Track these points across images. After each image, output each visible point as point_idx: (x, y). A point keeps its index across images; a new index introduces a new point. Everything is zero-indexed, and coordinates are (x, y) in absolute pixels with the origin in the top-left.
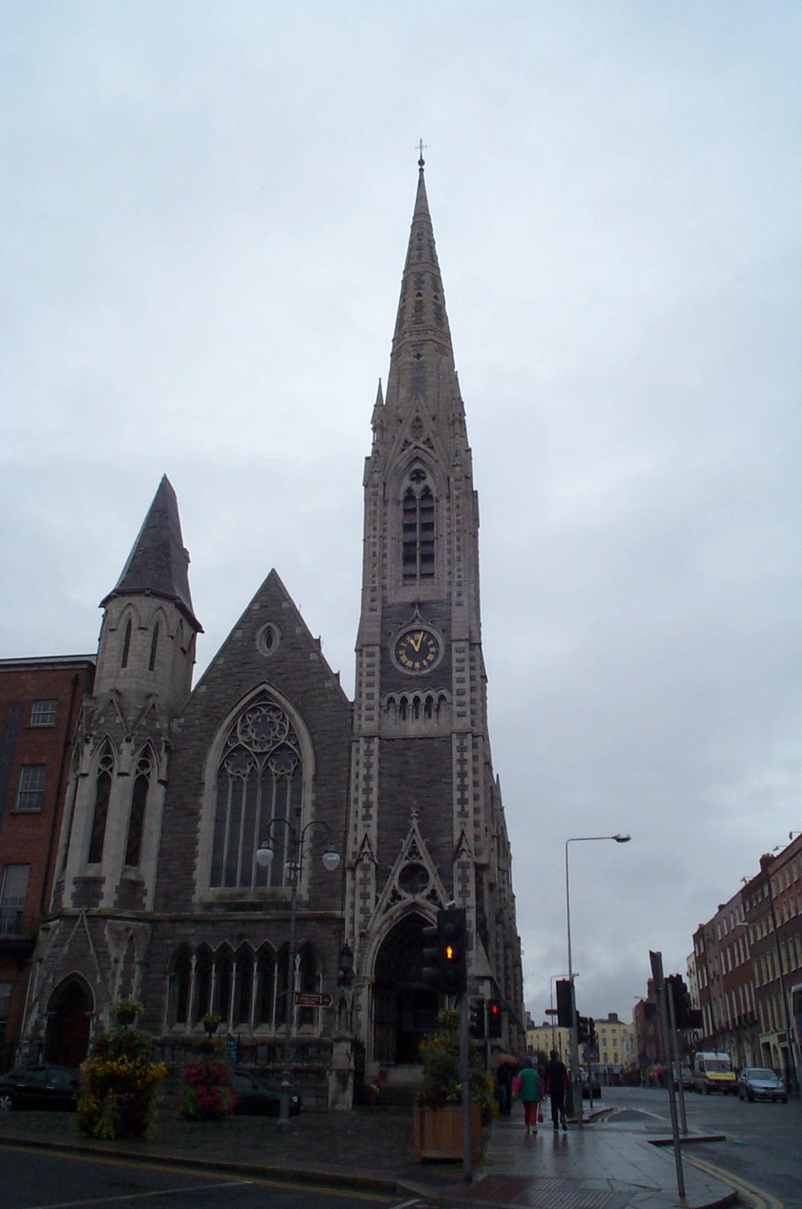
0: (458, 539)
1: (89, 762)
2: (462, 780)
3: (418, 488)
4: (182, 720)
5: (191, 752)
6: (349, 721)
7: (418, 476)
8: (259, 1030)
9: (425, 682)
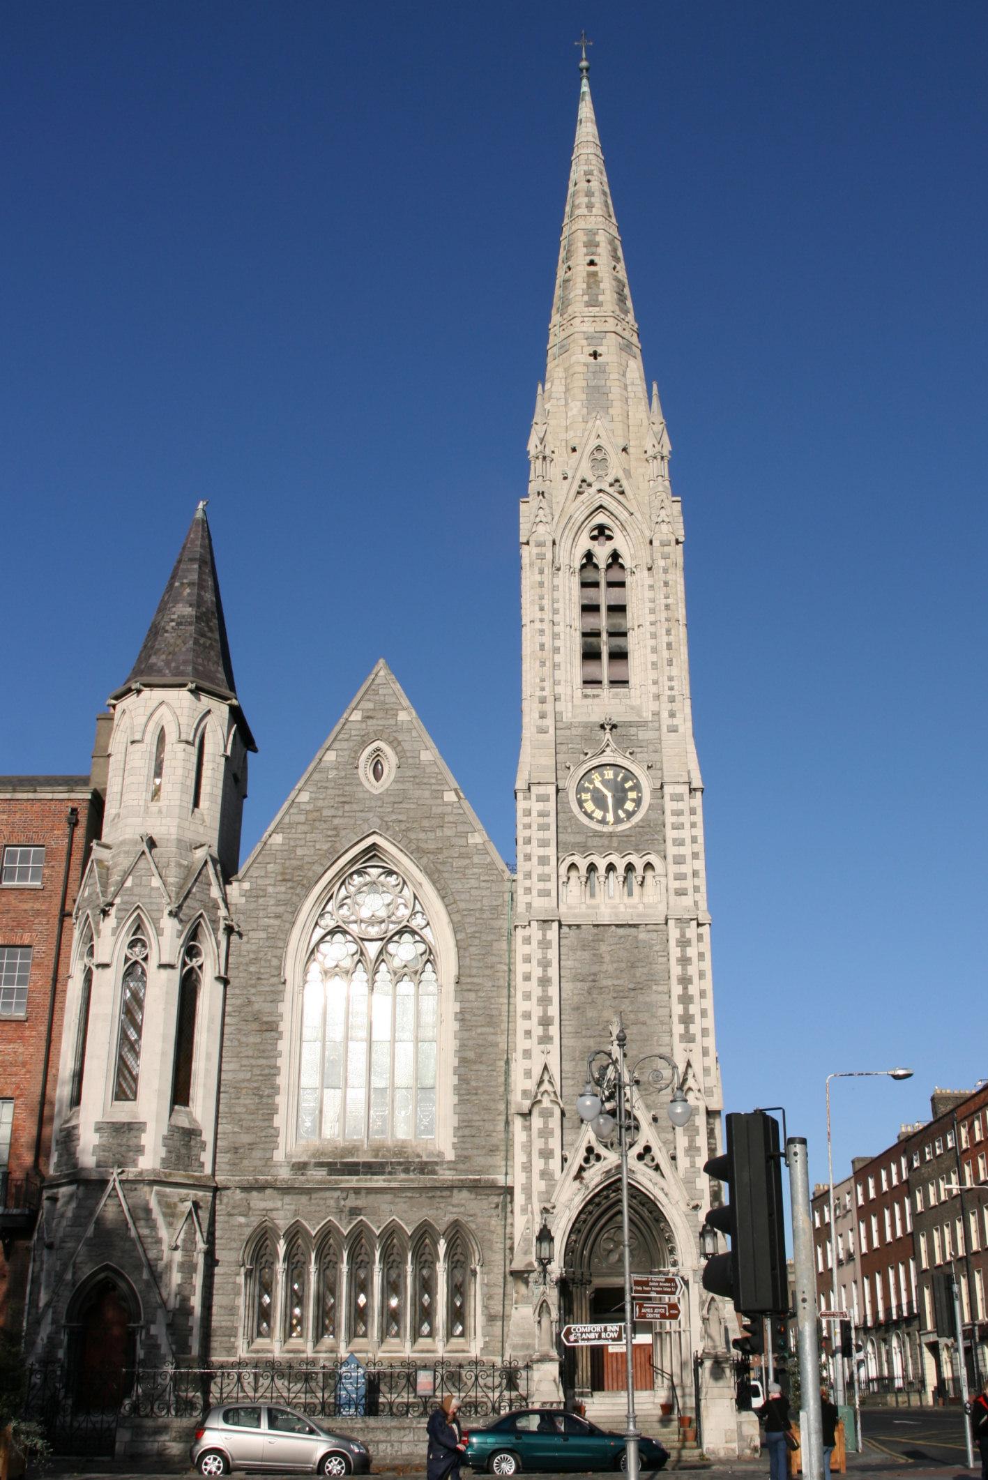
0: (668, 632)
1: (111, 943)
2: (685, 988)
3: (602, 553)
4: (246, 886)
5: (263, 935)
6: (507, 897)
7: (601, 532)
8: (384, 1347)
9: (625, 842)
